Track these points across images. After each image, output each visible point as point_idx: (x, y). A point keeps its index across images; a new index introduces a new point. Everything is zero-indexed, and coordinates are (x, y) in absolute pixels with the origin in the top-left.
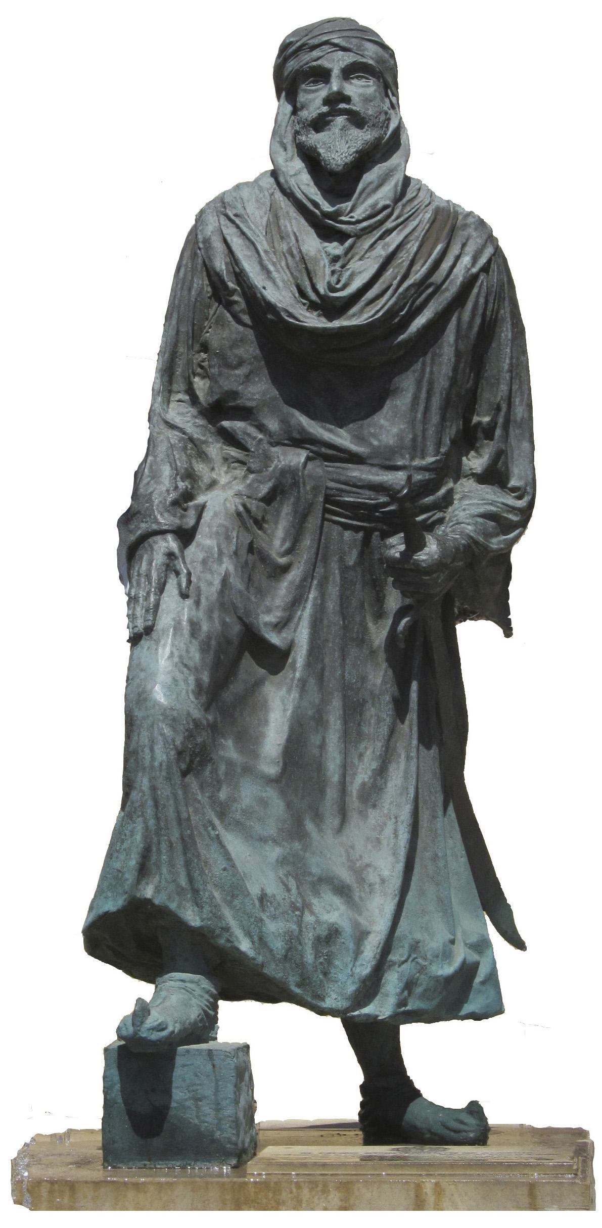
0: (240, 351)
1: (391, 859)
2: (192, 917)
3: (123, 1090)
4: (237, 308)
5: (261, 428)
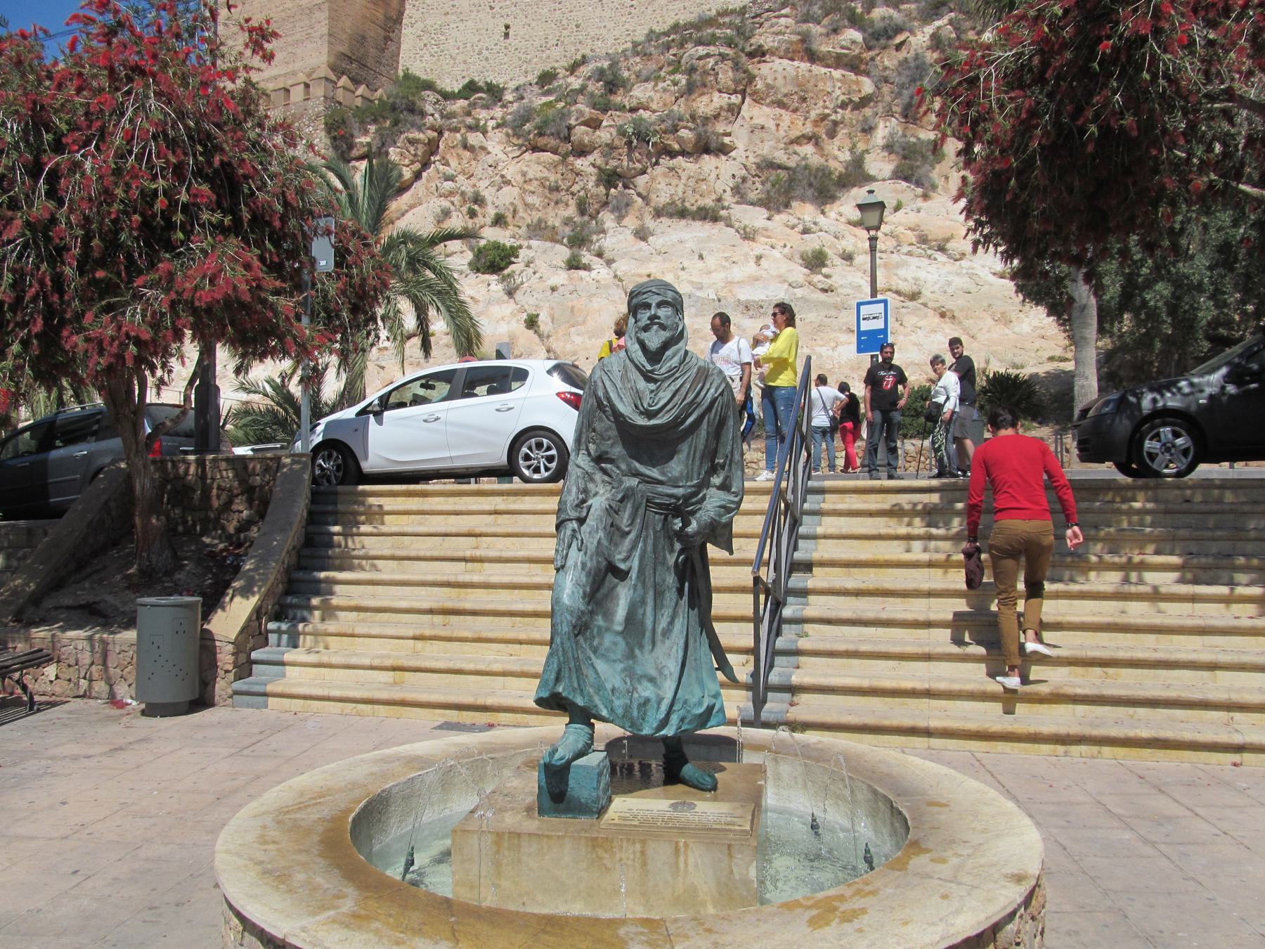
5: (618, 468)
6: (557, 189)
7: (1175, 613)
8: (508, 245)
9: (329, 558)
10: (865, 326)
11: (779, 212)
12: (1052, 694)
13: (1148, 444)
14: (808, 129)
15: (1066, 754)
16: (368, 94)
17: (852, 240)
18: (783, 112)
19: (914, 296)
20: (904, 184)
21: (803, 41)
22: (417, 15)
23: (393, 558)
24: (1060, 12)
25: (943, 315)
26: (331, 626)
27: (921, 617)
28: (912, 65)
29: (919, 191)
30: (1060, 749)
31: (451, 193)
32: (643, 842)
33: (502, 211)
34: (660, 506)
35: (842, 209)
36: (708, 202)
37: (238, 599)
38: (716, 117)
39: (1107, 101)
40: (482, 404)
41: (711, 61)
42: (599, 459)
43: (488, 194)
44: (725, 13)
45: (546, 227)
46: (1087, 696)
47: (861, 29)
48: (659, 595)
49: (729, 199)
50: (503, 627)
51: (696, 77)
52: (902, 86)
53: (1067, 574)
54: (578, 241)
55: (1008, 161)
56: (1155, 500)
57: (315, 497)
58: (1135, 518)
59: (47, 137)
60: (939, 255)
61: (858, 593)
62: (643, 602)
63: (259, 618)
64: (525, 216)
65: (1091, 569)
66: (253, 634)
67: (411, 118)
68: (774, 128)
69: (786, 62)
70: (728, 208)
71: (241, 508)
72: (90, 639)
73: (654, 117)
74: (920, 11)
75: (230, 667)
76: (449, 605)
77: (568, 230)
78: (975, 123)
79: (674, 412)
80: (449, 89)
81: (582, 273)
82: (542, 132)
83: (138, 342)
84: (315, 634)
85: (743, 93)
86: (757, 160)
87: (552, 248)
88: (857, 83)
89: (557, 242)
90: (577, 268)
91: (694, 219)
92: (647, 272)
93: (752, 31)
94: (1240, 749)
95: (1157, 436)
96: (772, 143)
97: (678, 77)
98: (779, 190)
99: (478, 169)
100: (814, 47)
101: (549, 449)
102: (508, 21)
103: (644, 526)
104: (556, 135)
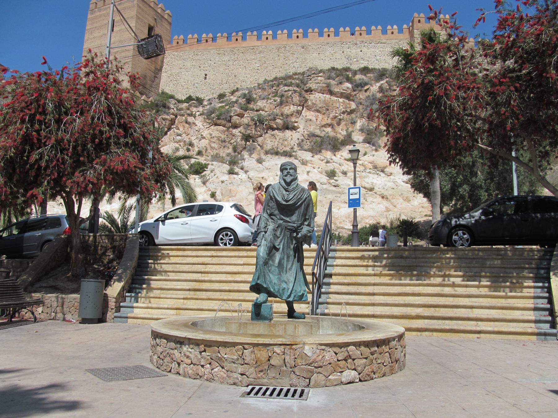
2: (265, 286)
6: (225, 141)
7: (460, 291)
8: (204, 163)
9: (148, 271)
10: (352, 197)
11: (317, 154)
12: (416, 316)
13: (454, 237)
14: (329, 121)
16: (146, 99)
17: (346, 166)
18: (319, 114)
19: (371, 190)
20: (368, 145)
21: (328, 87)
22: (168, 68)
23: (173, 272)
24: (416, 87)
25: (383, 197)
26: (151, 295)
27: (371, 292)
28: (371, 98)
29: (374, 148)
30: (419, 333)
31: (180, 141)
32: (285, 325)
33: (201, 149)
34: (289, 229)
35: (342, 154)
36: (288, 149)
37: (116, 283)
38: (292, 115)
39: (432, 115)
40: (204, 220)
41: (290, 93)
42: (271, 215)
43: (195, 142)
44: (295, 74)
45: (219, 157)
47: (351, 83)
48: (288, 257)
49: (296, 148)
50: (217, 295)
51: (284, 98)
52: (367, 106)
53: (423, 278)
54: (233, 163)
55: (400, 134)
56: (455, 254)
57: (141, 250)
58: (447, 260)
59: (63, 110)
60: (381, 174)
61: (349, 284)
62: (283, 259)
63: (123, 291)
64: (211, 152)
65: (431, 277)
66: (121, 297)
67: (164, 110)
68: (315, 120)
69: (320, 95)
70: (296, 152)
71: (110, 254)
72: (57, 297)
73: (266, 114)
74: (375, 77)
75: (114, 307)
76: (196, 287)
77: (228, 158)
78: (389, 121)
79: (295, 201)
80: (180, 99)
81: (235, 176)
82: (219, 118)
83: (93, 183)
84: (145, 297)
85: (303, 106)
86: (308, 133)
87: (222, 165)
88: (349, 104)
89: (224, 163)
90: (233, 174)
91: (281, 156)
92: (262, 176)
93: (307, 81)
94: (479, 332)
95: (457, 234)
96: (314, 126)
97: (276, 98)
98: (317, 146)
99: (191, 132)
100: (332, 89)
101: (230, 236)
102: (206, 73)
103: (284, 235)
104: (225, 119)
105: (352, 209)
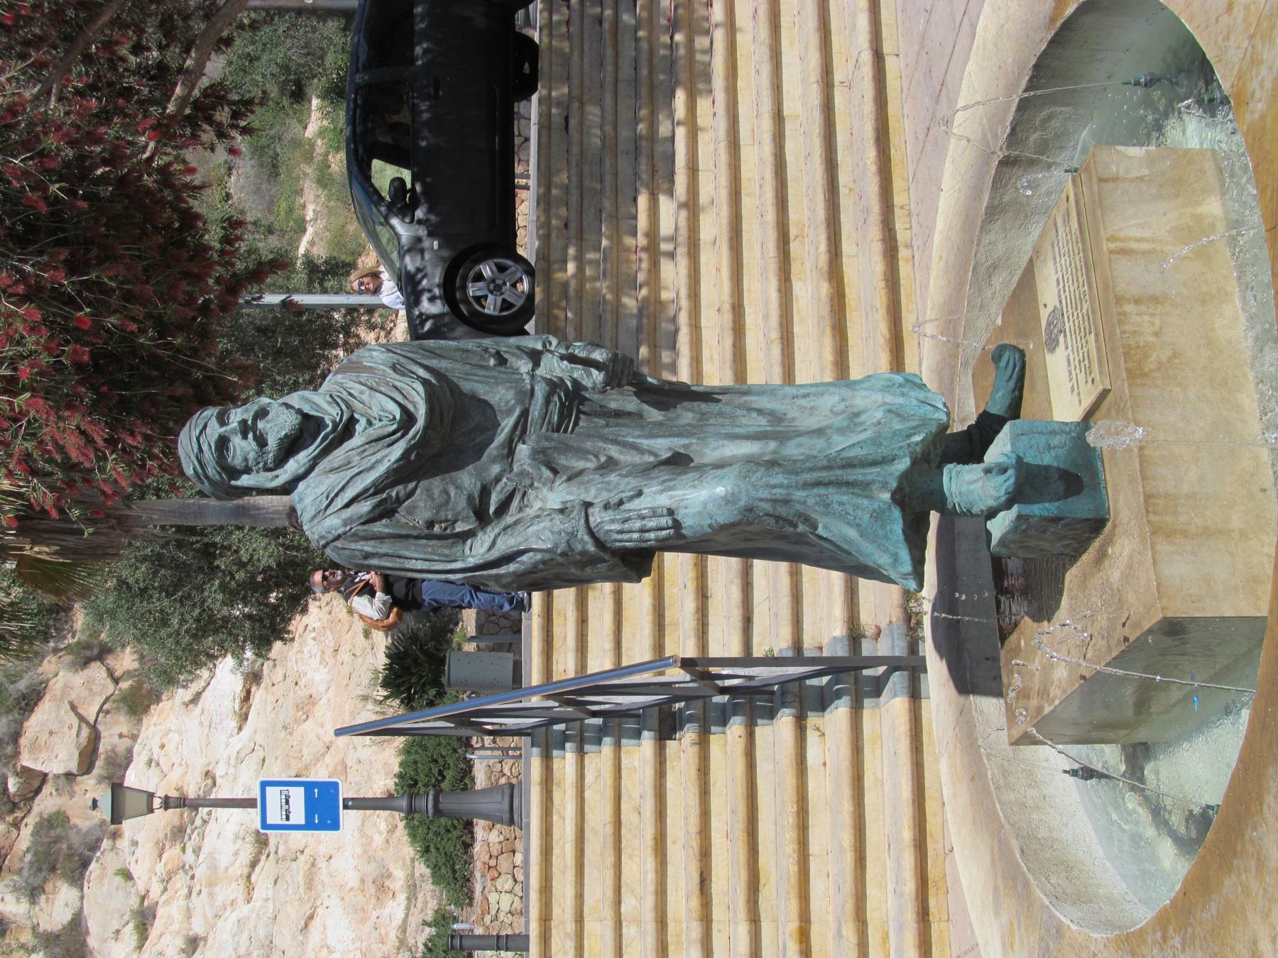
0: (436, 492)
1: (826, 397)
2: (903, 464)
3: (1050, 501)
4: (402, 493)
5: (498, 479)
10: (298, 816)
12: (830, 280)
15: (909, 246)
17: (167, 938)
29: (106, 844)
30: (903, 253)
46: (829, 238)
95: (479, 277)
105: (349, 818)
